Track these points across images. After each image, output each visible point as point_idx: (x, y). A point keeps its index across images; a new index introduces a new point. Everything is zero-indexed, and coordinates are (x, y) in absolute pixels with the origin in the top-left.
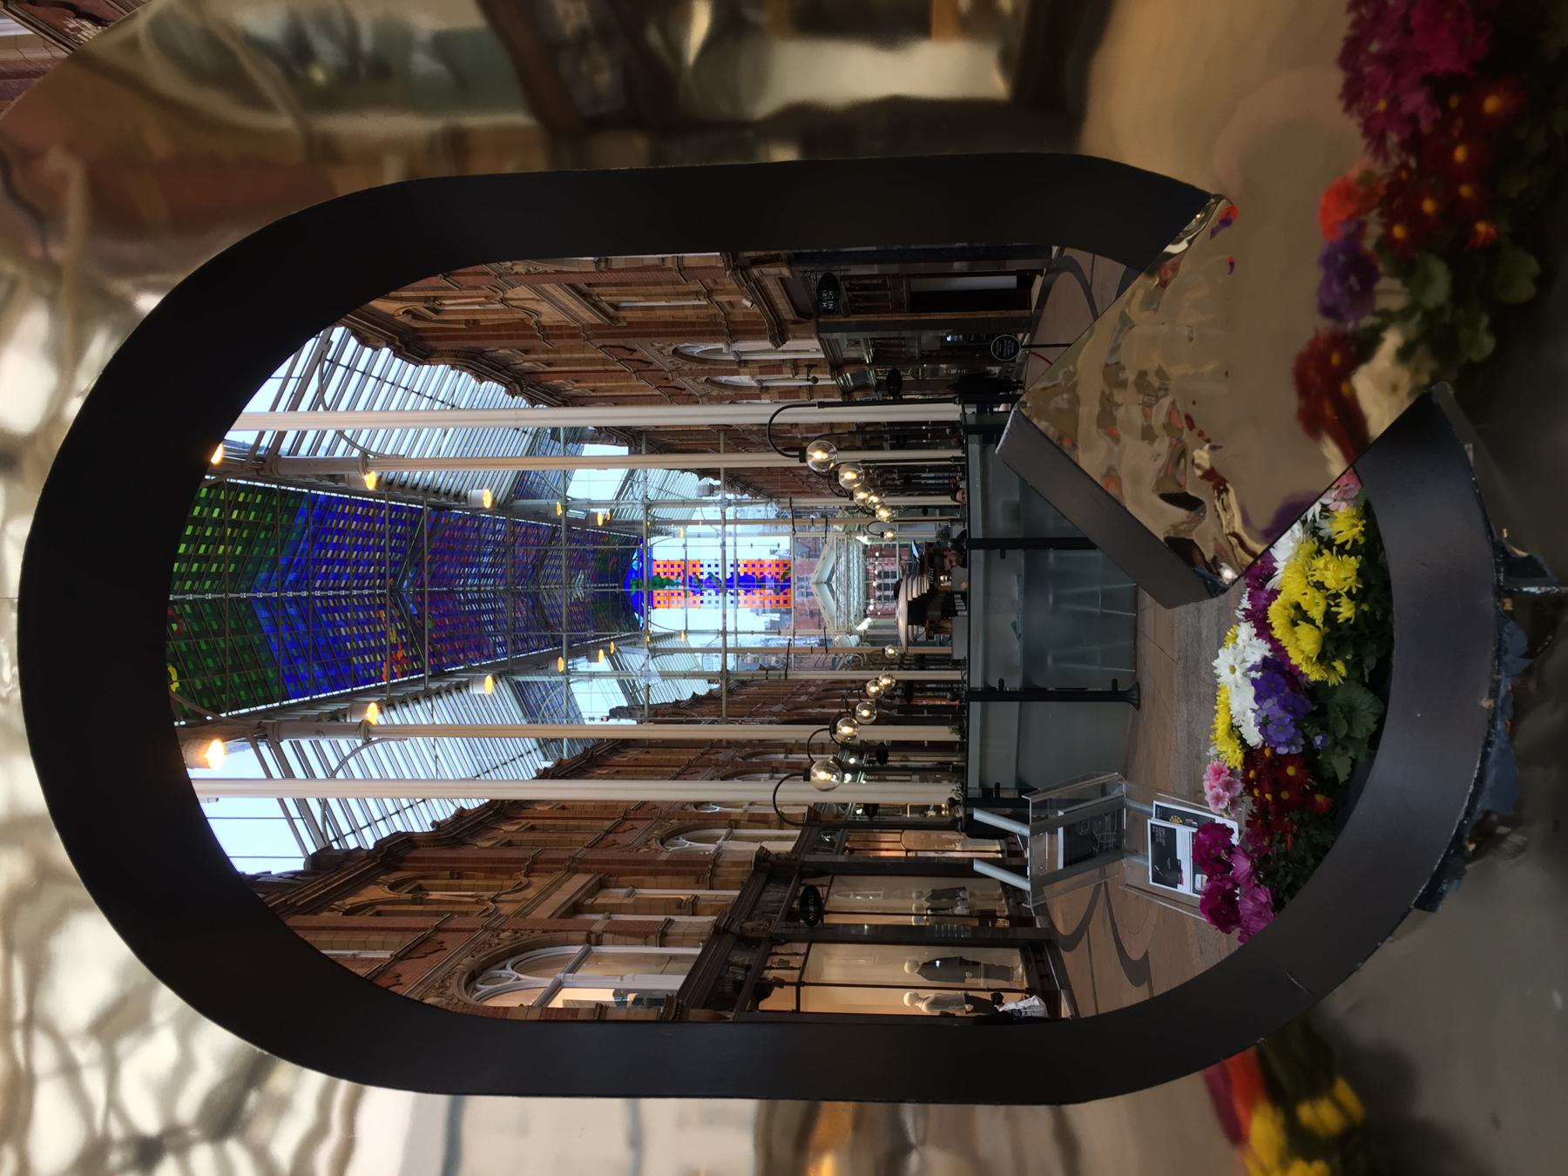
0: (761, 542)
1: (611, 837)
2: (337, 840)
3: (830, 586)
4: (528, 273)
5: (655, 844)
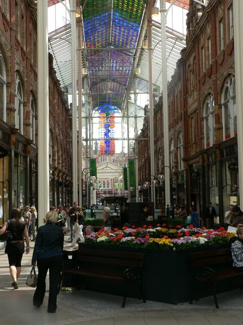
0: (122, 147)
3: (106, 167)
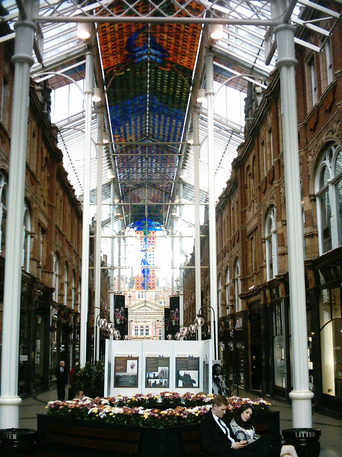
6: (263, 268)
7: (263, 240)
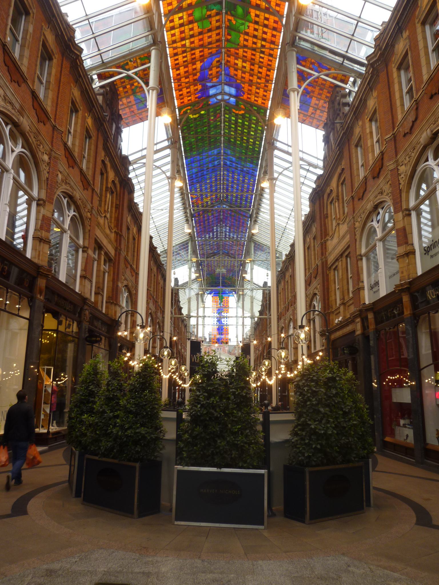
1: (129, 267)
2: (134, 169)
4: (355, 228)
5: (125, 283)
6: (359, 291)
7: (360, 257)
